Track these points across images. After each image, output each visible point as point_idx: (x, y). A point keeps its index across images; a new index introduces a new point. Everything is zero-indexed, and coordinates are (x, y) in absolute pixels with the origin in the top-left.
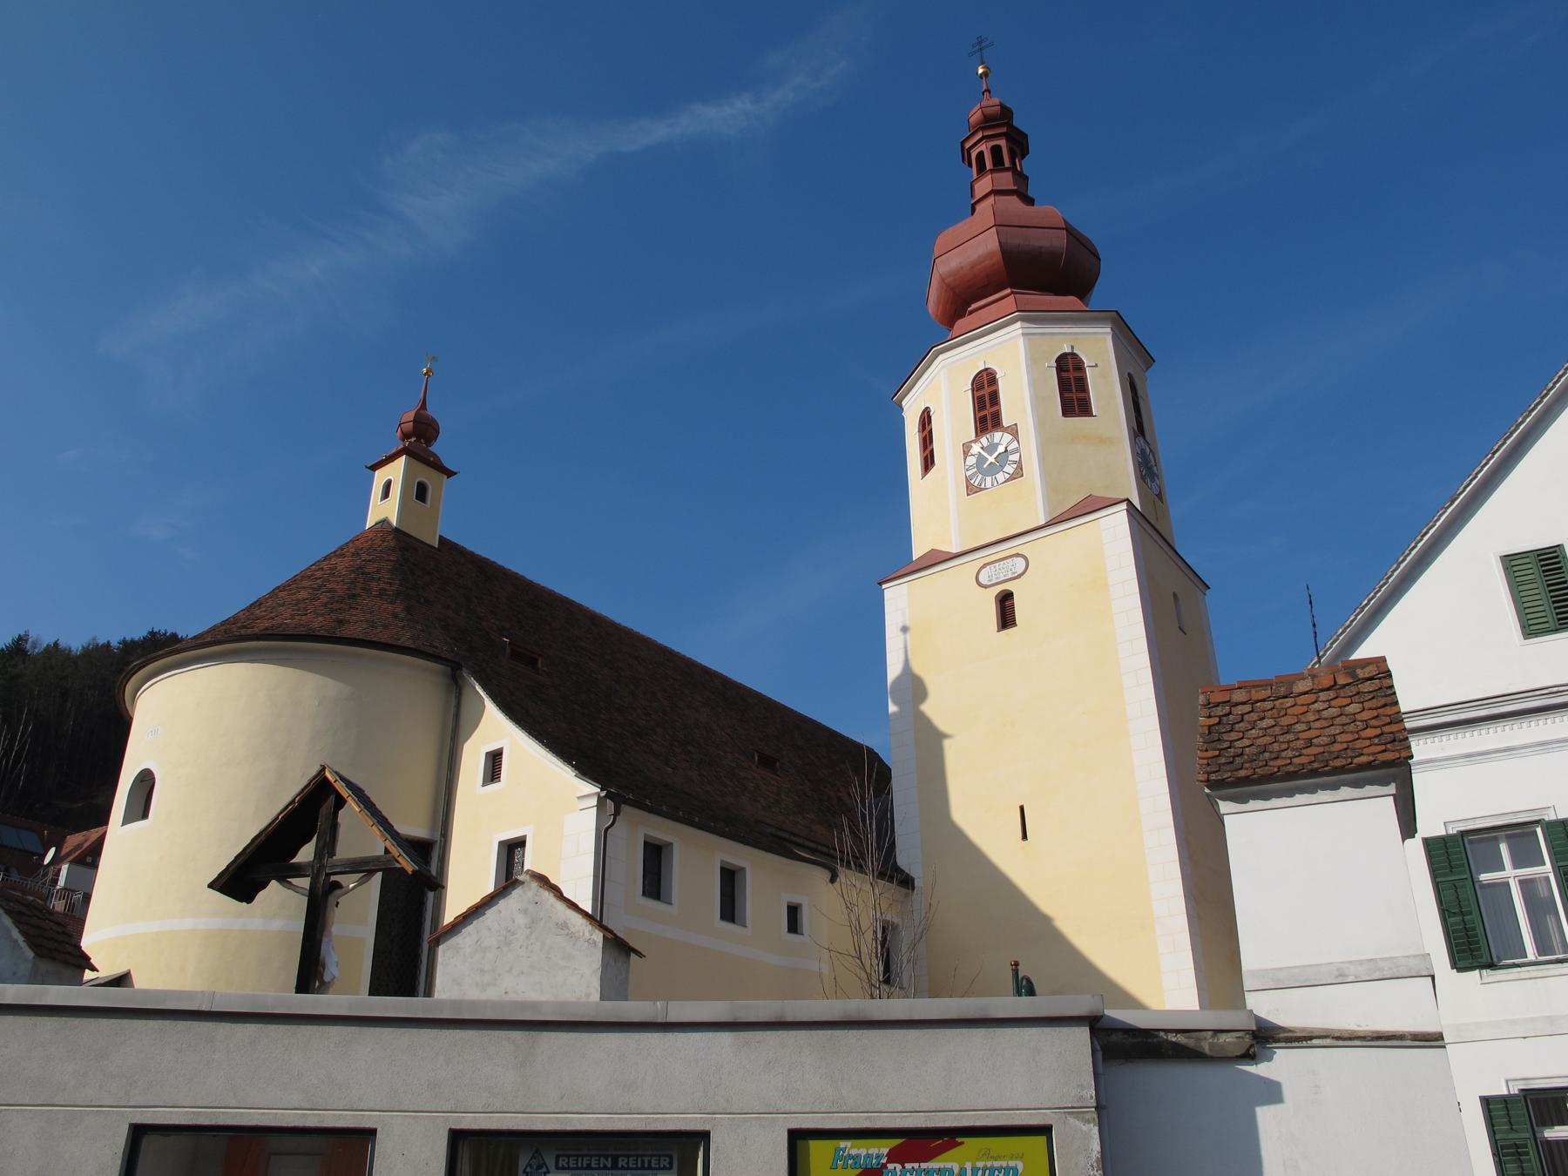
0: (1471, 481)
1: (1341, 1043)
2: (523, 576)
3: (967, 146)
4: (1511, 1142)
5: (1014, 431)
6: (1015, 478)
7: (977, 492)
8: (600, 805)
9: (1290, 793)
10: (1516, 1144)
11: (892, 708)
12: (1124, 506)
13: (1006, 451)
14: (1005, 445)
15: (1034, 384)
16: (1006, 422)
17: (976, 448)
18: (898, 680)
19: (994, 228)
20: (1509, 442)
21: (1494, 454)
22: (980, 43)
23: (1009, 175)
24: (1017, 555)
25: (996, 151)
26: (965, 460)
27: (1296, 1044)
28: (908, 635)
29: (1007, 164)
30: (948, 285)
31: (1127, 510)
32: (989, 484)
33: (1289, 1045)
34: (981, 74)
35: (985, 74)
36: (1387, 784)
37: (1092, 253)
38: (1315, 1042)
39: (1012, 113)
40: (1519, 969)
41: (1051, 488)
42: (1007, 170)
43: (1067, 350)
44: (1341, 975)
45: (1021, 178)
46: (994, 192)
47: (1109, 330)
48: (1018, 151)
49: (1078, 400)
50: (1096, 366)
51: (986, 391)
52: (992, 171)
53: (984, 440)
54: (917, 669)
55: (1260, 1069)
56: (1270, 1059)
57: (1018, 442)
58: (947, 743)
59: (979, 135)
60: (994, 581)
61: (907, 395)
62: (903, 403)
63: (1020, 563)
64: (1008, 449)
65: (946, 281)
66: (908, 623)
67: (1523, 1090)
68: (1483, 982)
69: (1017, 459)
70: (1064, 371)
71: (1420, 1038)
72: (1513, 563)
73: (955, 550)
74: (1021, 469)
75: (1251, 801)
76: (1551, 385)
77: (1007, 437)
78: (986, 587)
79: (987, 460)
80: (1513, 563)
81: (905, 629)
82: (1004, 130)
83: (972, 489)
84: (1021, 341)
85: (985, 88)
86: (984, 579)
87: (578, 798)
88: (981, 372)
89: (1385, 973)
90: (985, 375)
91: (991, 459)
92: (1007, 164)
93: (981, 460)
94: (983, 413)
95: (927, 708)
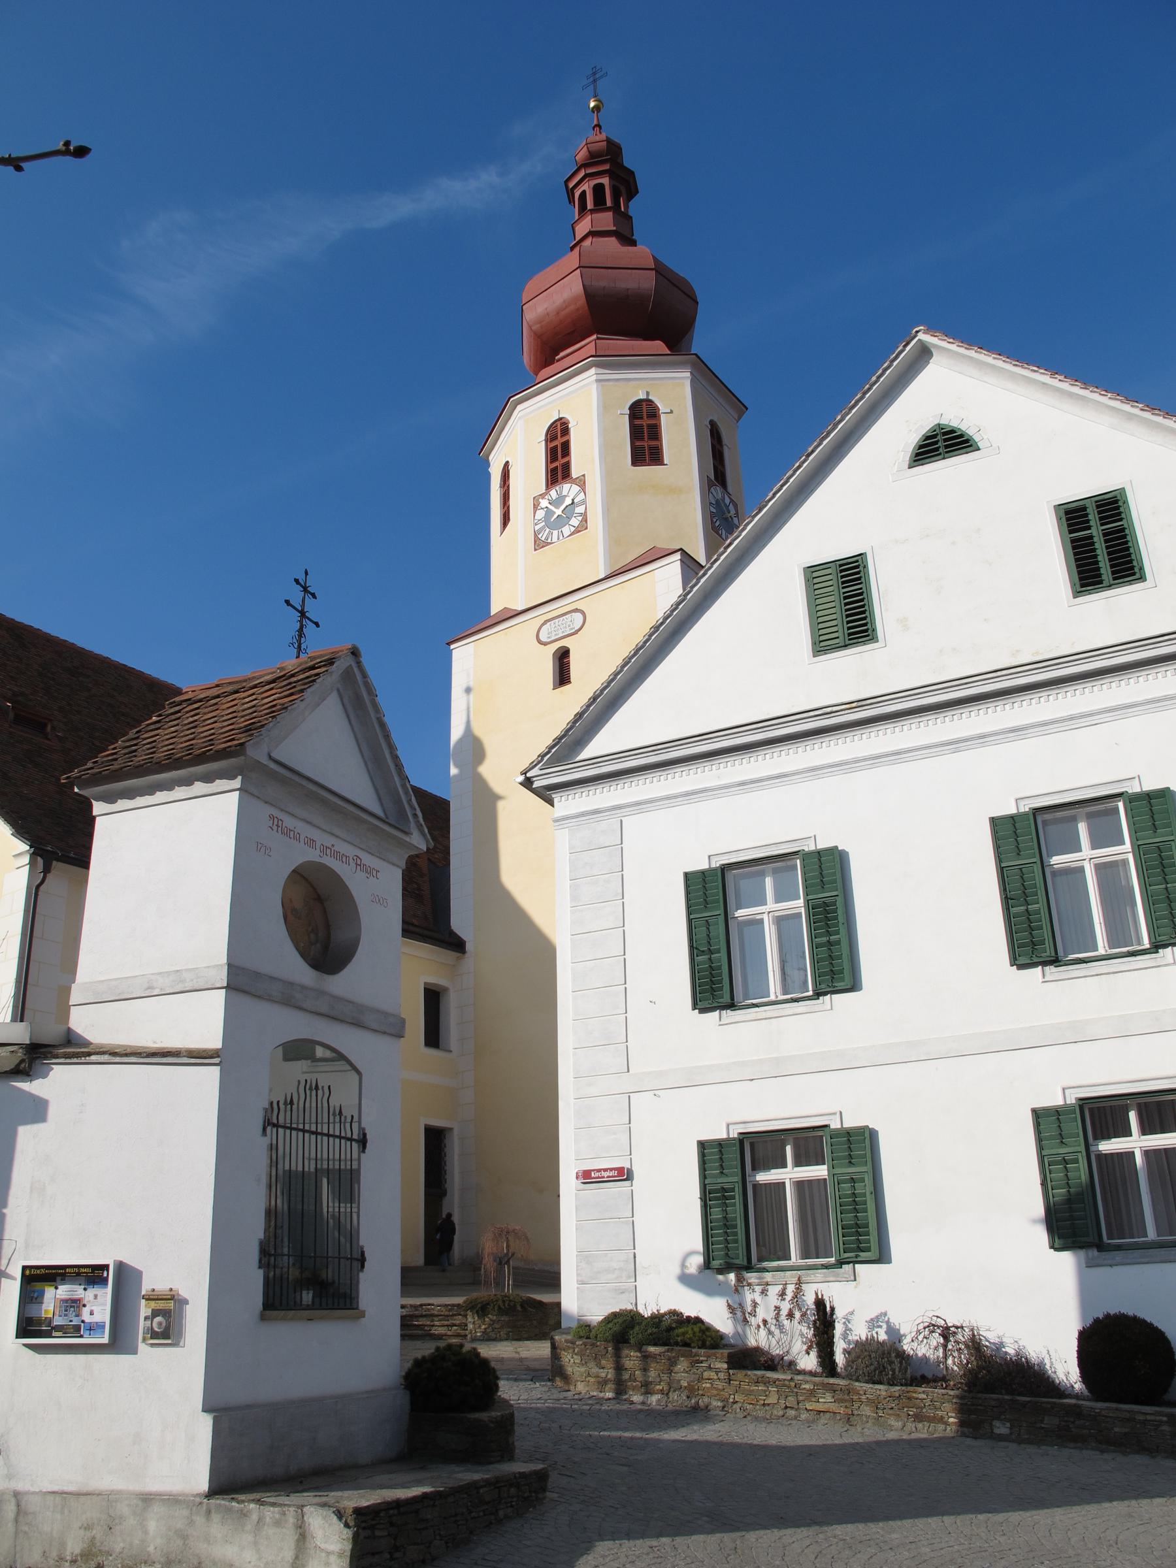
0: (782, 486)
1: (117, 1059)
2: (73, 644)
3: (571, 185)
4: (718, 1186)
5: (581, 482)
6: (580, 531)
7: (543, 547)
8: (32, 864)
9: (150, 790)
10: (723, 1188)
11: (454, 771)
12: (678, 556)
13: (573, 503)
14: (572, 497)
15: (604, 432)
16: (575, 472)
17: (544, 503)
18: (460, 741)
19: (579, 270)
20: (825, 442)
21: (809, 455)
22: (594, 74)
23: (609, 215)
24: (576, 610)
25: (599, 190)
26: (535, 513)
27: (75, 1060)
28: (472, 696)
29: (609, 203)
30: (535, 333)
31: (680, 560)
32: (555, 539)
33: (68, 1061)
34: (594, 107)
35: (597, 109)
36: (233, 778)
37: (688, 296)
38: (93, 1058)
39: (621, 149)
40: (757, 1009)
41: (614, 539)
42: (609, 209)
43: (642, 396)
44: (149, 988)
45: (624, 218)
46: (592, 234)
47: (688, 374)
48: (623, 189)
49: (650, 448)
50: (671, 412)
51: (558, 443)
52: (592, 211)
53: (553, 493)
54: (478, 731)
55: (34, 1087)
56: (45, 1076)
57: (585, 494)
58: (501, 805)
59: (582, 174)
60: (553, 638)
61: (493, 449)
62: (490, 458)
63: (578, 617)
64: (576, 501)
65: (533, 328)
66: (471, 684)
67: (741, 1133)
68: (721, 1023)
69: (583, 512)
70: (638, 418)
71: (194, 1054)
72: (815, 574)
73: (520, 608)
74: (586, 521)
75: (119, 800)
76: (874, 378)
77: (576, 488)
78: (545, 644)
79: (555, 513)
80: (815, 574)
81: (468, 690)
82: (607, 167)
83: (539, 544)
84: (595, 386)
85: (595, 122)
86: (543, 638)
87: (13, 856)
88: (556, 421)
89: (186, 985)
90: (559, 426)
91: (558, 512)
92: (609, 203)
93: (549, 513)
94: (554, 465)
95: (485, 770)
